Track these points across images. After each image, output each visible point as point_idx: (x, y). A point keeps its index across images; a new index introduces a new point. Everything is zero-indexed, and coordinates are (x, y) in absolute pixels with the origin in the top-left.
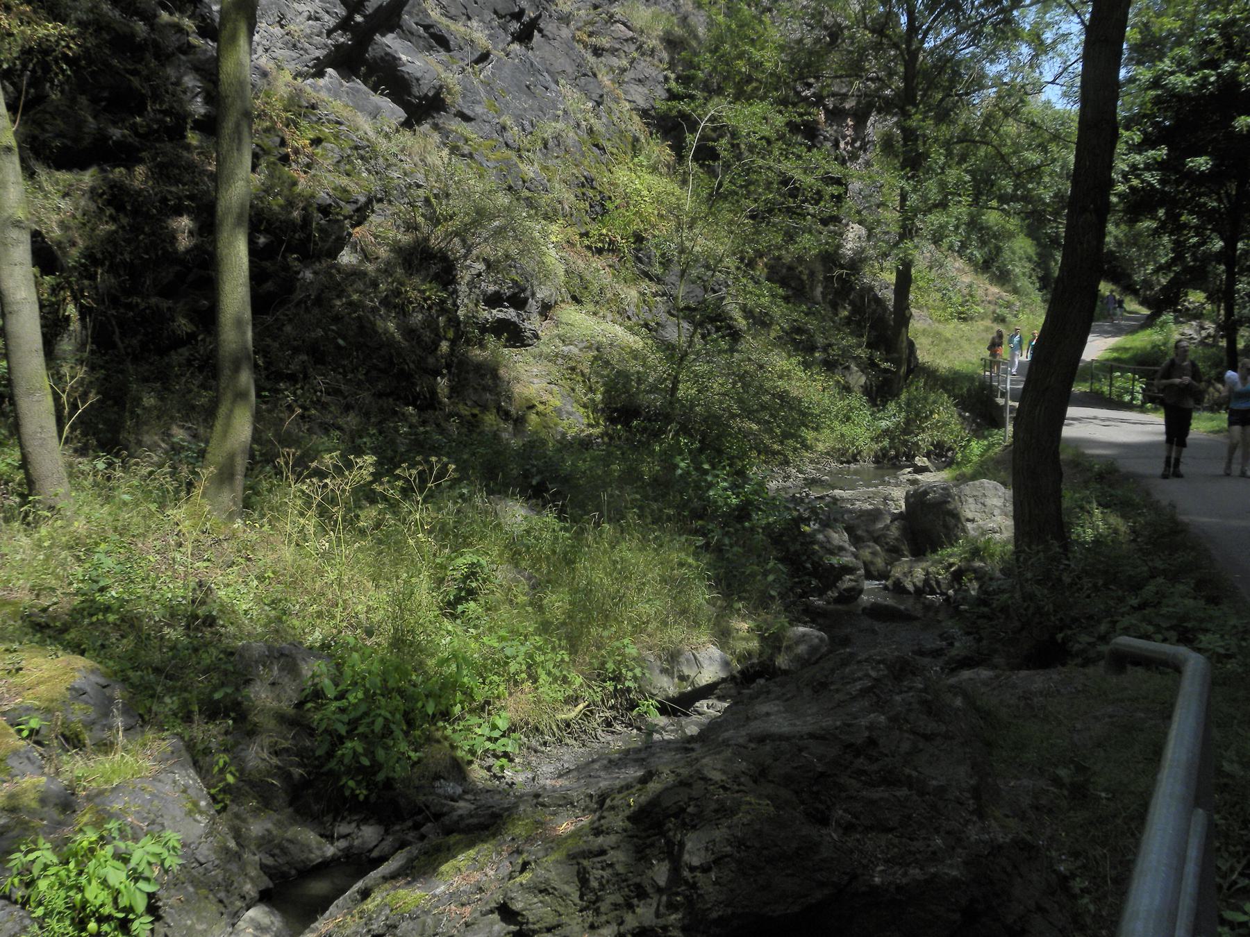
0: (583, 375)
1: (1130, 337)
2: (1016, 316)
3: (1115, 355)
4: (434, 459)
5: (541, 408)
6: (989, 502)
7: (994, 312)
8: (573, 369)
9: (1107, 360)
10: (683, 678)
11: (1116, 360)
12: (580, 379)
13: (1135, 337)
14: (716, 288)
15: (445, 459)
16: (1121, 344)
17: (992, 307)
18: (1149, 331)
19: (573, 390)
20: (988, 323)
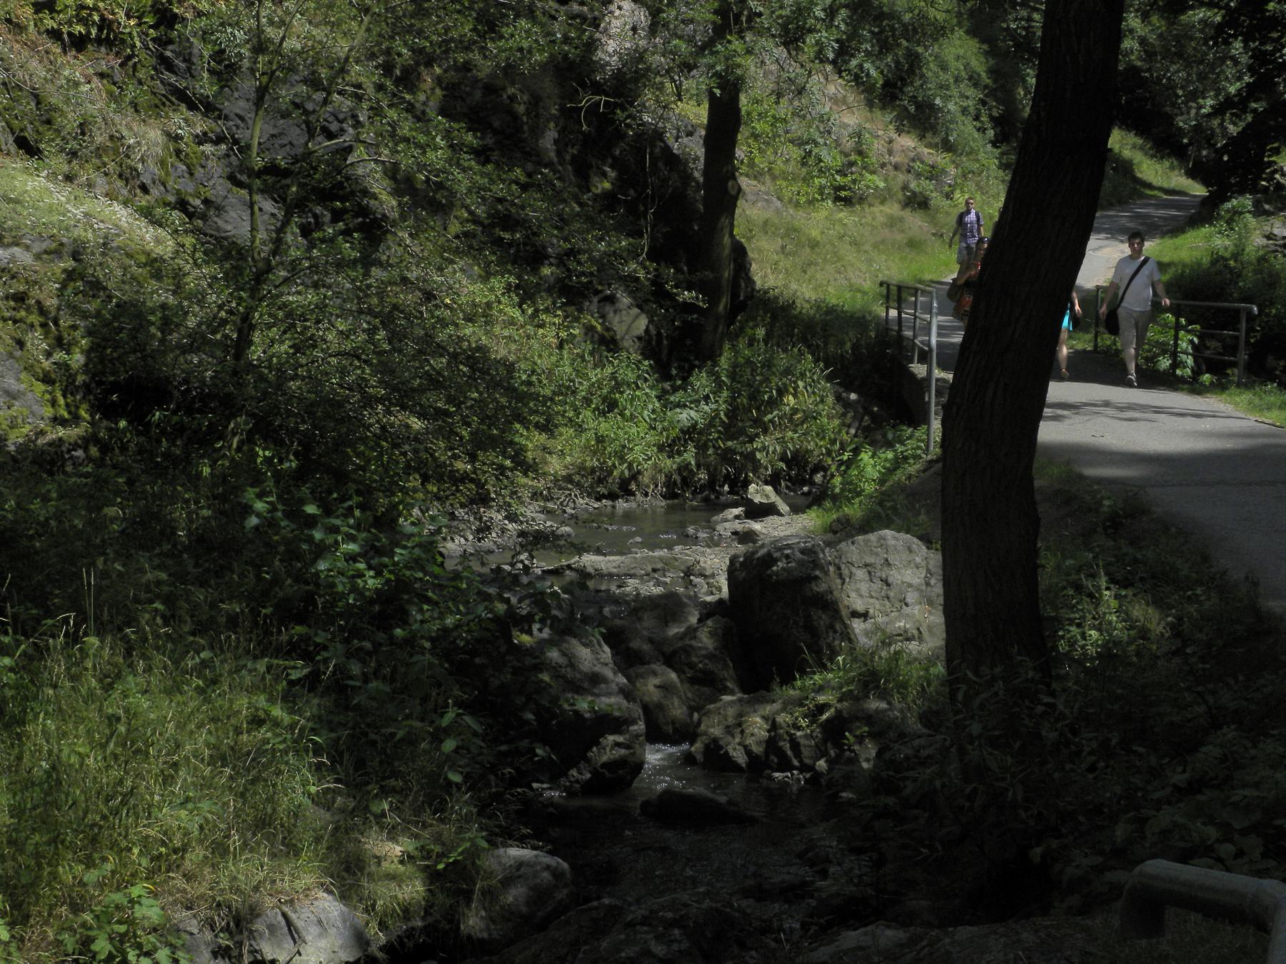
0: (42, 311)
1: (1169, 242)
2: (948, 196)
6: (895, 576)
7: (905, 187)
8: (20, 298)
12: (35, 318)
13: (1180, 240)
14: (334, 127)
17: (902, 177)
18: (1206, 230)
19: (20, 344)
20: (893, 209)
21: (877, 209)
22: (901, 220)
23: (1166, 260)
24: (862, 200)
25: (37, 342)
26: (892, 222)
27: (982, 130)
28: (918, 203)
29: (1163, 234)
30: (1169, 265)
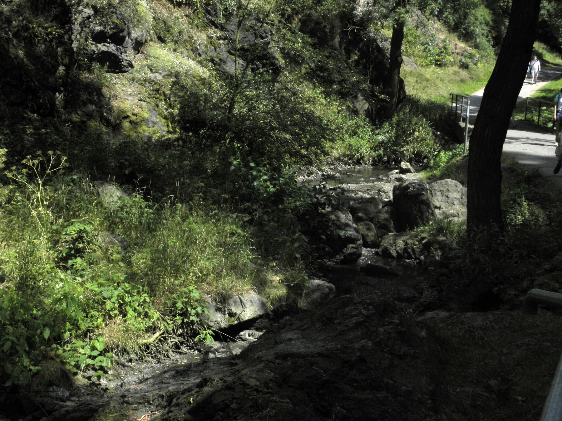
1: (554, 82)
2: (476, 64)
3: (544, 94)
4: (50, 152)
5: (133, 118)
6: (451, 195)
7: (460, 61)
8: (157, 90)
9: (538, 98)
10: (231, 315)
11: (543, 98)
13: (558, 82)
15: (58, 153)
16: (546, 87)
17: (459, 57)
19: (157, 106)
20: (456, 68)
21: (450, 68)
22: (459, 72)
23: (552, 88)
24: (445, 65)
25: (163, 105)
26: (455, 73)
27: (489, 41)
28: (465, 66)
29: (552, 80)
30: (554, 90)
